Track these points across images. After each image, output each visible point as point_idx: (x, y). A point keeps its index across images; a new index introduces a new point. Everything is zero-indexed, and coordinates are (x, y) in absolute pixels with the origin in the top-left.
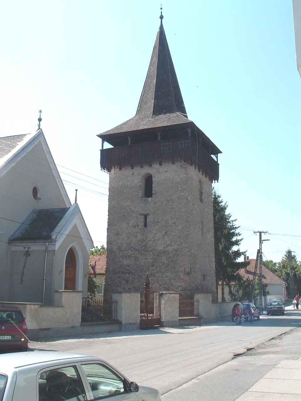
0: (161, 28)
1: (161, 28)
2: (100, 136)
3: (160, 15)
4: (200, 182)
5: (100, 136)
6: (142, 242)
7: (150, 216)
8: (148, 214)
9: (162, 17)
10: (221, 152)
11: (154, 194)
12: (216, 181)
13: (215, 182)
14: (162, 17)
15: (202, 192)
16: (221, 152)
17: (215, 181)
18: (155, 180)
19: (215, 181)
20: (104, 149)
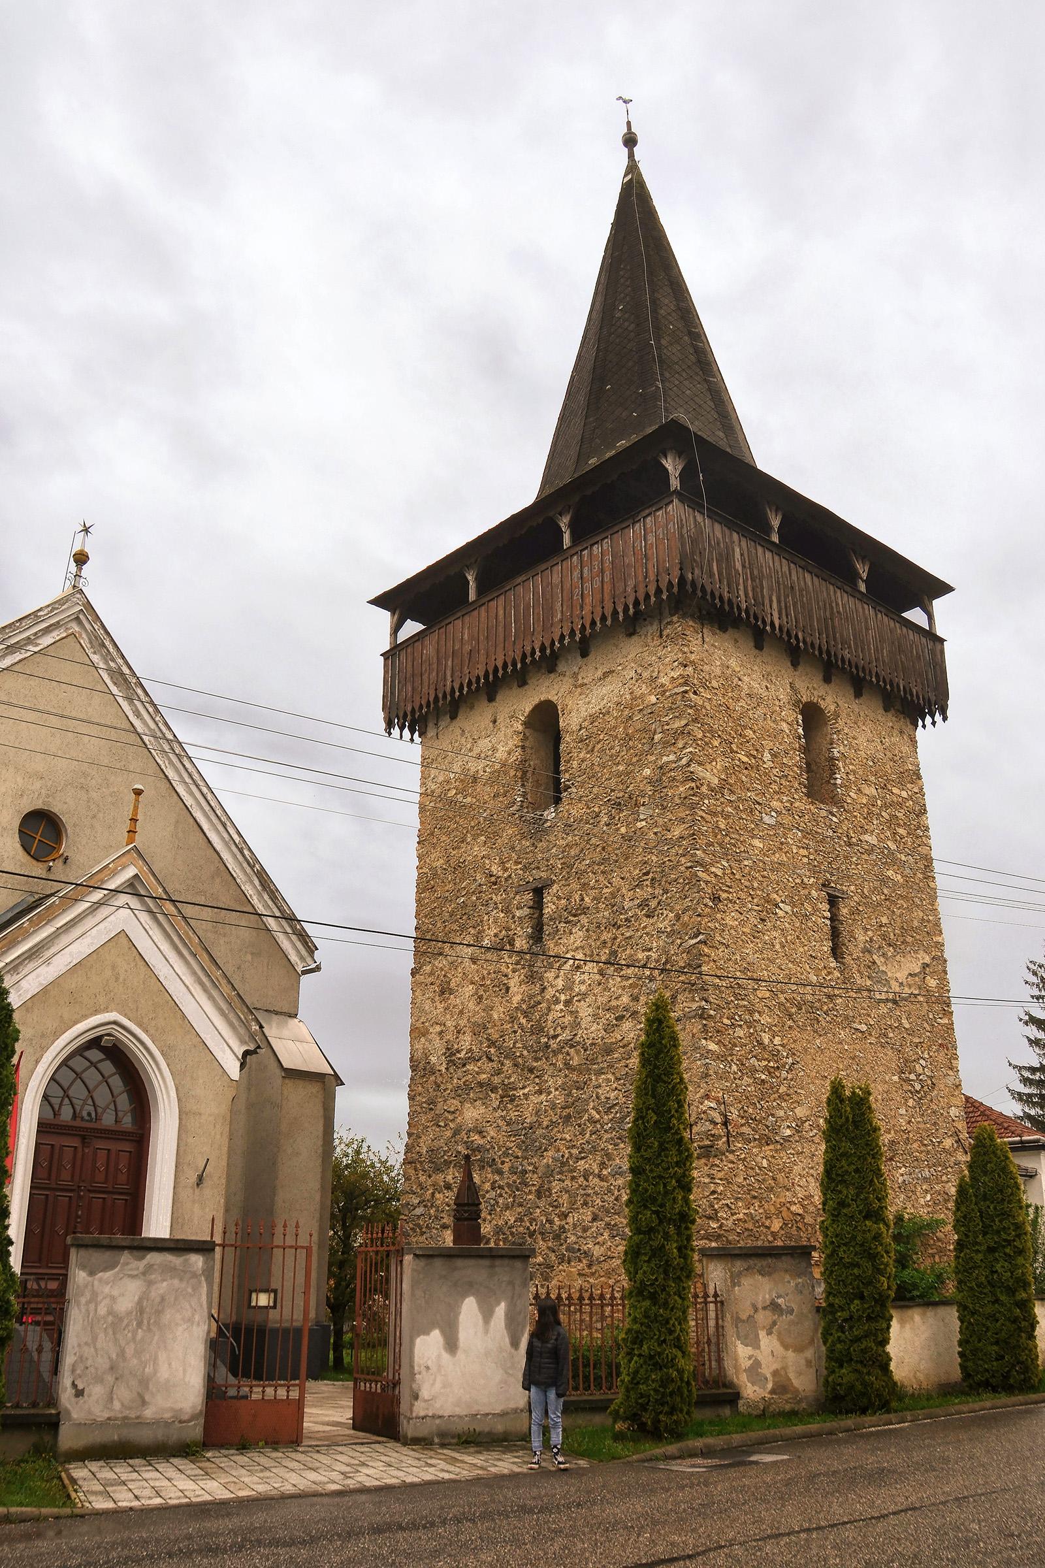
0: (632, 167)
1: (632, 167)
2: (382, 601)
3: (625, 130)
4: (812, 716)
5: (382, 601)
6: (526, 1014)
7: (555, 887)
8: (549, 884)
9: (630, 141)
10: (943, 588)
11: (707, 1152)
12: (938, 717)
13: (934, 723)
14: (630, 141)
15: (833, 759)
16: (943, 588)
17: (933, 717)
18: (571, 720)
19: (933, 717)
20: (104, 1057)
